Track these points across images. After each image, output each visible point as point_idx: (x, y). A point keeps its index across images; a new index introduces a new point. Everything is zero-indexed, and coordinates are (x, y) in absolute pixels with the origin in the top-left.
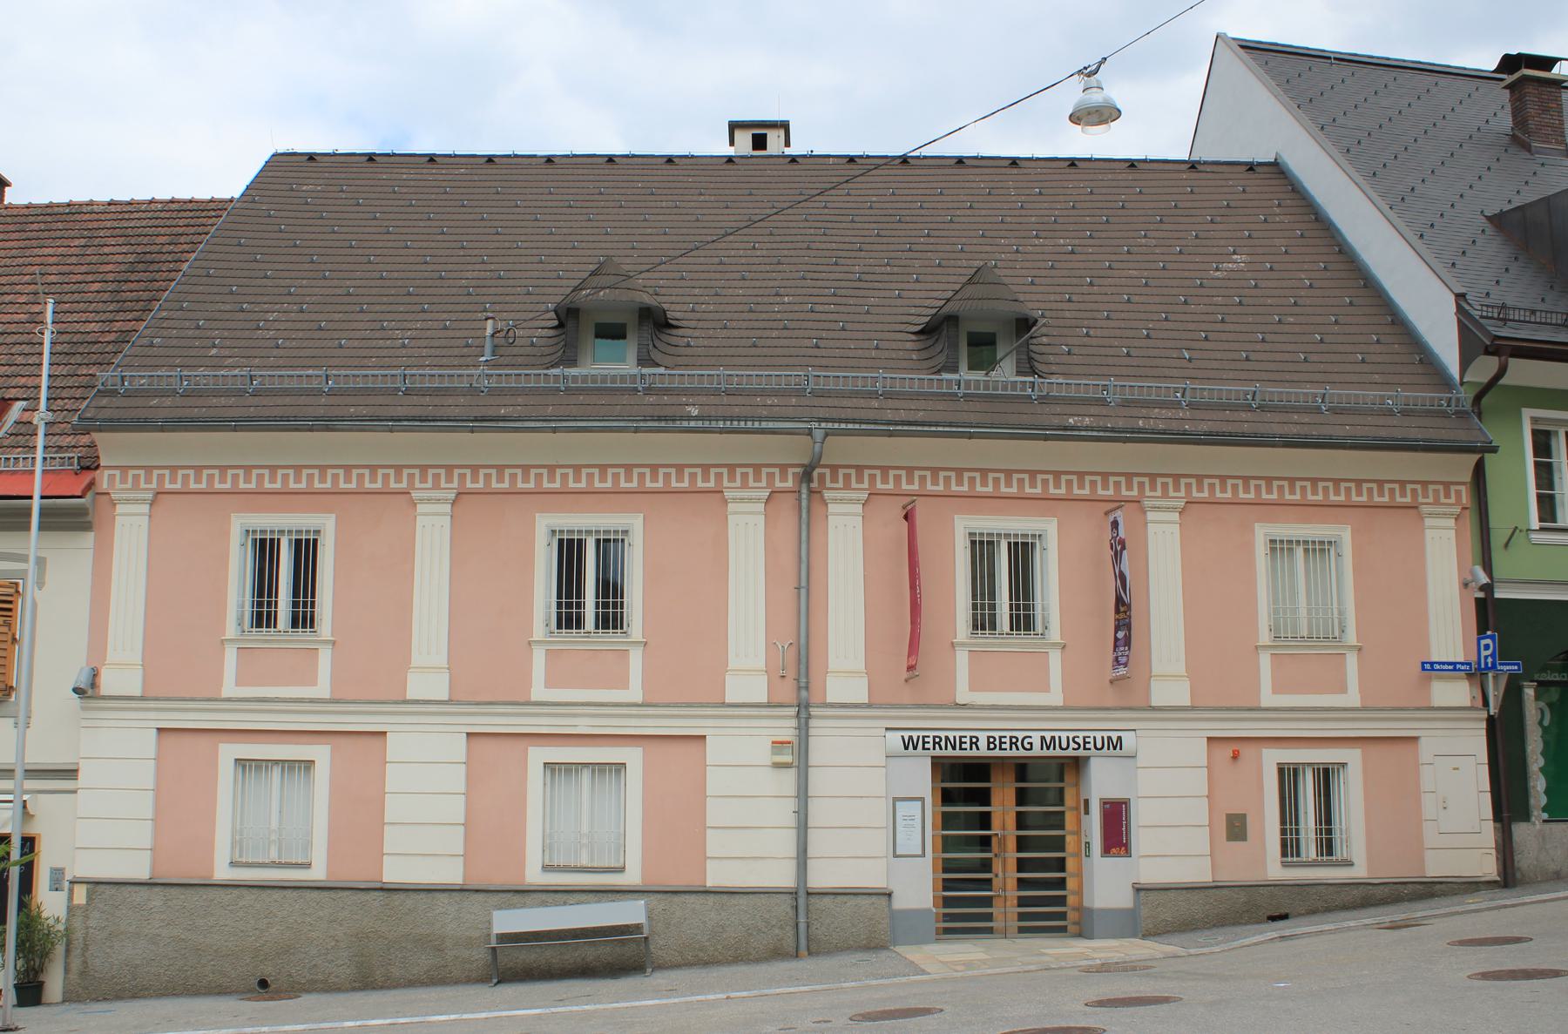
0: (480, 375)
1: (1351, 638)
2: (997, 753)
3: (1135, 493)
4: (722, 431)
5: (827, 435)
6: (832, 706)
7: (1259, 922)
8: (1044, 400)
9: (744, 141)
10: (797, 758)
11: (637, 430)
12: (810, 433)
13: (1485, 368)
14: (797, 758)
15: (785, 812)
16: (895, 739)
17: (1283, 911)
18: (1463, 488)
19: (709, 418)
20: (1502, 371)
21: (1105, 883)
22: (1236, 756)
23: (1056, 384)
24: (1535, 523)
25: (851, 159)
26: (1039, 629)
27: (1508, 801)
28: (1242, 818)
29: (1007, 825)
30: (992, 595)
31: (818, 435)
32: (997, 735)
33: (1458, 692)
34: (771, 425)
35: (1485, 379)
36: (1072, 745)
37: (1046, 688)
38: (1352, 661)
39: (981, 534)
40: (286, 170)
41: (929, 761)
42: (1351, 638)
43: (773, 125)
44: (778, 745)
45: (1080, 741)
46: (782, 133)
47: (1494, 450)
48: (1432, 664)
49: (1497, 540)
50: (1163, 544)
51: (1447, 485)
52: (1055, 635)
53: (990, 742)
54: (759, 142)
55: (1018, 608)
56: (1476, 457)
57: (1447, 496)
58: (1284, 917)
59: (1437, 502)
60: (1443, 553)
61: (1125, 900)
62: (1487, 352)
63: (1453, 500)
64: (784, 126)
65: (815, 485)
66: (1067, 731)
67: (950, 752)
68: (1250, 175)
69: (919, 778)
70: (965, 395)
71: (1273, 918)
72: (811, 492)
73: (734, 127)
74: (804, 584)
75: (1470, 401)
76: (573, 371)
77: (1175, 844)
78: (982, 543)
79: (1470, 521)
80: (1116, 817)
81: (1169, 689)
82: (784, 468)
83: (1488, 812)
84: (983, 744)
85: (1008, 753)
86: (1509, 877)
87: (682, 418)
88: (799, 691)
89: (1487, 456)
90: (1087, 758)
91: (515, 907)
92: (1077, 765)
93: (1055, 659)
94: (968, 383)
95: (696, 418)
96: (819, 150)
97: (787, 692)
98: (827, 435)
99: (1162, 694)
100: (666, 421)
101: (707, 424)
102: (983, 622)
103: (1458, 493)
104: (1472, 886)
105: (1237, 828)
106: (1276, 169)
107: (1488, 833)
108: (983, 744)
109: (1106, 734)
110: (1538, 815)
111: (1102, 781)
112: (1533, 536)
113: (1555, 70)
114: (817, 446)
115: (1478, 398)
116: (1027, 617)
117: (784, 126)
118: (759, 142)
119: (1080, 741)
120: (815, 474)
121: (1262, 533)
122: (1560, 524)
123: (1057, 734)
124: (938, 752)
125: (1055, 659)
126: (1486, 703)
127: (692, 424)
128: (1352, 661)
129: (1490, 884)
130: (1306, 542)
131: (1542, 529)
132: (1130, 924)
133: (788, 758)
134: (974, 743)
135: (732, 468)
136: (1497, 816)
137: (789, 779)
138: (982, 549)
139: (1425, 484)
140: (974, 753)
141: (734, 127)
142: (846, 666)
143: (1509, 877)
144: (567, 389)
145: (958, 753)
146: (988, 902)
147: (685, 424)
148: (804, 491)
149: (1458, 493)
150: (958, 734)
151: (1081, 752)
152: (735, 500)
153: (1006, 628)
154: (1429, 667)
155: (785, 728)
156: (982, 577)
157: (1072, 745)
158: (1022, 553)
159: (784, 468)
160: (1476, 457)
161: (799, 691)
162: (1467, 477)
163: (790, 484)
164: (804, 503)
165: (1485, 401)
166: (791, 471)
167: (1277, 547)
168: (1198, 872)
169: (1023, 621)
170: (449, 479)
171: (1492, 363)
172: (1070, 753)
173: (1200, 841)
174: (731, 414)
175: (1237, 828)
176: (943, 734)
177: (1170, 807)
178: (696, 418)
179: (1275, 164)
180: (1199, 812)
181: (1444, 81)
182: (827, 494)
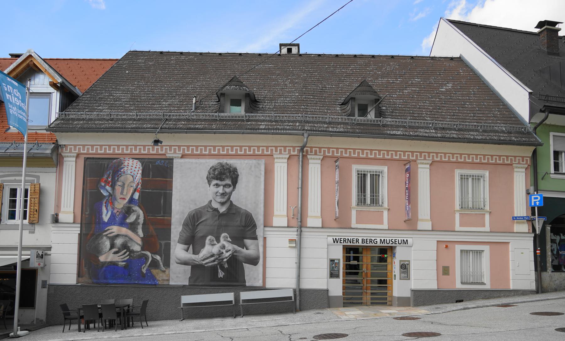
0: (191, 114)
1: (487, 208)
2: (365, 244)
3: (415, 158)
4: (273, 134)
5: (309, 135)
6: (309, 227)
7: (453, 303)
8: (384, 126)
9: (284, 51)
10: (298, 244)
11: (243, 133)
12: (303, 135)
13: (538, 119)
14: (298, 244)
15: (292, 262)
16: (330, 240)
17: (461, 299)
18: (528, 159)
19: (269, 129)
20: (546, 118)
21: (399, 288)
22: (447, 247)
23: (388, 120)
24: (552, 171)
25: (319, 55)
26: (380, 203)
27: (540, 265)
28: (448, 267)
29: (364, 272)
30: (365, 192)
31: (306, 135)
32: (365, 238)
33: (525, 227)
34: (290, 132)
35: (538, 122)
36: (391, 242)
37: (382, 223)
38: (487, 217)
39: (361, 171)
40: (133, 55)
41: (342, 247)
42: (487, 208)
43: (294, 45)
44: (291, 241)
45: (393, 241)
46: (297, 47)
47: (541, 145)
48: (516, 217)
49: (540, 177)
50: (424, 174)
51: (523, 157)
52: (386, 205)
53: (363, 240)
54: (289, 50)
55: (373, 196)
56: (534, 148)
57: (523, 161)
58: (462, 301)
59: (519, 163)
60: (520, 180)
61: (408, 294)
62: (541, 111)
63: (525, 163)
64: (298, 45)
65: (305, 153)
66: (389, 237)
67: (349, 244)
68: (452, 61)
69: (338, 254)
70: (357, 124)
71: (457, 302)
72: (303, 156)
73: (281, 45)
74: (300, 186)
75: (532, 129)
76: (222, 114)
77: (424, 277)
78: (361, 174)
79: (530, 171)
80: (405, 267)
81: (425, 224)
82: (294, 147)
83: (533, 268)
84: (360, 241)
85: (369, 245)
86: (540, 289)
87: (259, 129)
88: (299, 221)
89: (539, 148)
90: (395, 247)
91: (201, 294)
92: (392, 249)
93: (385, 213)
94: (358, 120)
95: (264, 129)
96: (309, 52)
97: (295, 223)
98: (309, 135)
99: (421, 226)
100: (254, 130)
101: (267, 131)
102: (362, 201)
103: (527, 160)
104: (524, 293)
105: (446, 271)
106: (460, 60)
107: (532, 275)
108: (360, 241)
109: (402, 239)
110: (550, 269)
111: (400, 254)
112: (551, 175)
113: (557, 26)
114: (305, 140)
115: (535, 128)
116: (376, 199)
117: (298, 45)
118: (289, 50)
119: (393, 241)
120: (305, 149)
121: (458, 172)
122: (560, 172)
123: (385, 239)
124: (345, 244)
125: (385, 213)
126: (534, 230)
127: (263, 131)
128: (487, 217)
129: (531, 292)
130: (473, 176)
131: (555, 173)
132: (403, 302)
133: (294, 245)
134: (357, 241)
135: (276, 147)
136: (536, 270)
137: (294, 253)
138: (362, 177)
139: (515, 157)
140: (357, 244)
141: (281, 45)
142: (314, 218)
143: (540, 289)
144: (220, 119)
145: (352, 244)
146: (361, 294)
147: (260, 131)
148: (301, 155)
149: (527, 160)
150: (352, 238)
151: (394, 245)
152: (277, 158)
153: (369, 203)
154: (515, 218)
155: (293, 235)
156: (361, 181)
157: (391, 242)
158: (375, 177)
159: (294, 147)
160: (534, 148)
161: (299, 221)
162: (530, 155)
163: (296, 153)
164: (301, 159)
165: (538, 129)
166: (296, 148)
167: (464, 178)
168: (433, 286)
169: (375, 201)
170: (179, 150)
171: (543, 115)
172: (390, 245)
173: (433, 274)
174: (275, 128)
175: (446, 271)
176: (347, 238)
177: (419, 264)
178: (264, 129)
179: (460, 58)
180: (433, 265)
181: (515, 34)
182: (309, 157)
